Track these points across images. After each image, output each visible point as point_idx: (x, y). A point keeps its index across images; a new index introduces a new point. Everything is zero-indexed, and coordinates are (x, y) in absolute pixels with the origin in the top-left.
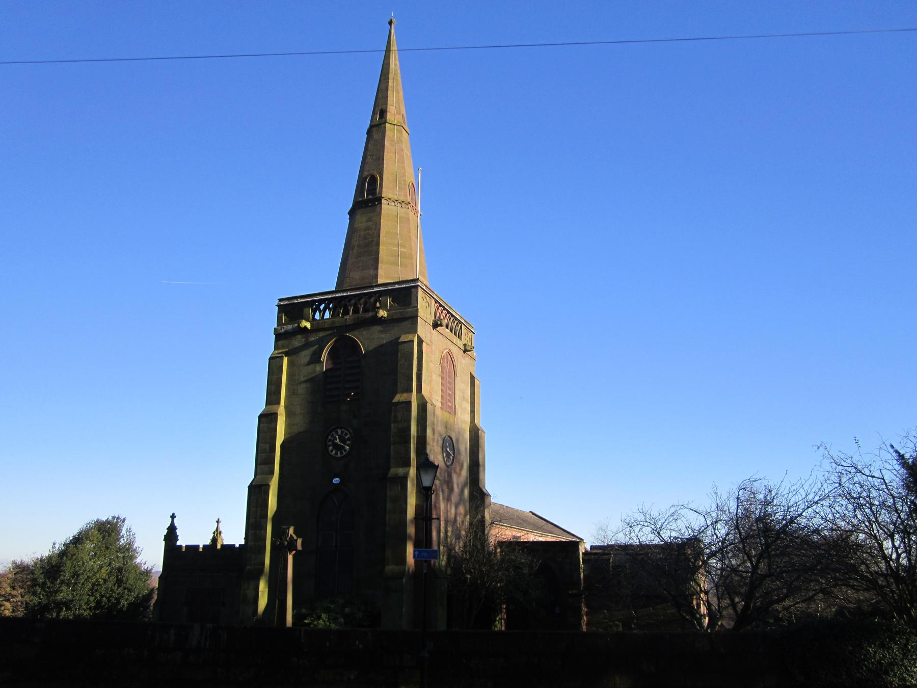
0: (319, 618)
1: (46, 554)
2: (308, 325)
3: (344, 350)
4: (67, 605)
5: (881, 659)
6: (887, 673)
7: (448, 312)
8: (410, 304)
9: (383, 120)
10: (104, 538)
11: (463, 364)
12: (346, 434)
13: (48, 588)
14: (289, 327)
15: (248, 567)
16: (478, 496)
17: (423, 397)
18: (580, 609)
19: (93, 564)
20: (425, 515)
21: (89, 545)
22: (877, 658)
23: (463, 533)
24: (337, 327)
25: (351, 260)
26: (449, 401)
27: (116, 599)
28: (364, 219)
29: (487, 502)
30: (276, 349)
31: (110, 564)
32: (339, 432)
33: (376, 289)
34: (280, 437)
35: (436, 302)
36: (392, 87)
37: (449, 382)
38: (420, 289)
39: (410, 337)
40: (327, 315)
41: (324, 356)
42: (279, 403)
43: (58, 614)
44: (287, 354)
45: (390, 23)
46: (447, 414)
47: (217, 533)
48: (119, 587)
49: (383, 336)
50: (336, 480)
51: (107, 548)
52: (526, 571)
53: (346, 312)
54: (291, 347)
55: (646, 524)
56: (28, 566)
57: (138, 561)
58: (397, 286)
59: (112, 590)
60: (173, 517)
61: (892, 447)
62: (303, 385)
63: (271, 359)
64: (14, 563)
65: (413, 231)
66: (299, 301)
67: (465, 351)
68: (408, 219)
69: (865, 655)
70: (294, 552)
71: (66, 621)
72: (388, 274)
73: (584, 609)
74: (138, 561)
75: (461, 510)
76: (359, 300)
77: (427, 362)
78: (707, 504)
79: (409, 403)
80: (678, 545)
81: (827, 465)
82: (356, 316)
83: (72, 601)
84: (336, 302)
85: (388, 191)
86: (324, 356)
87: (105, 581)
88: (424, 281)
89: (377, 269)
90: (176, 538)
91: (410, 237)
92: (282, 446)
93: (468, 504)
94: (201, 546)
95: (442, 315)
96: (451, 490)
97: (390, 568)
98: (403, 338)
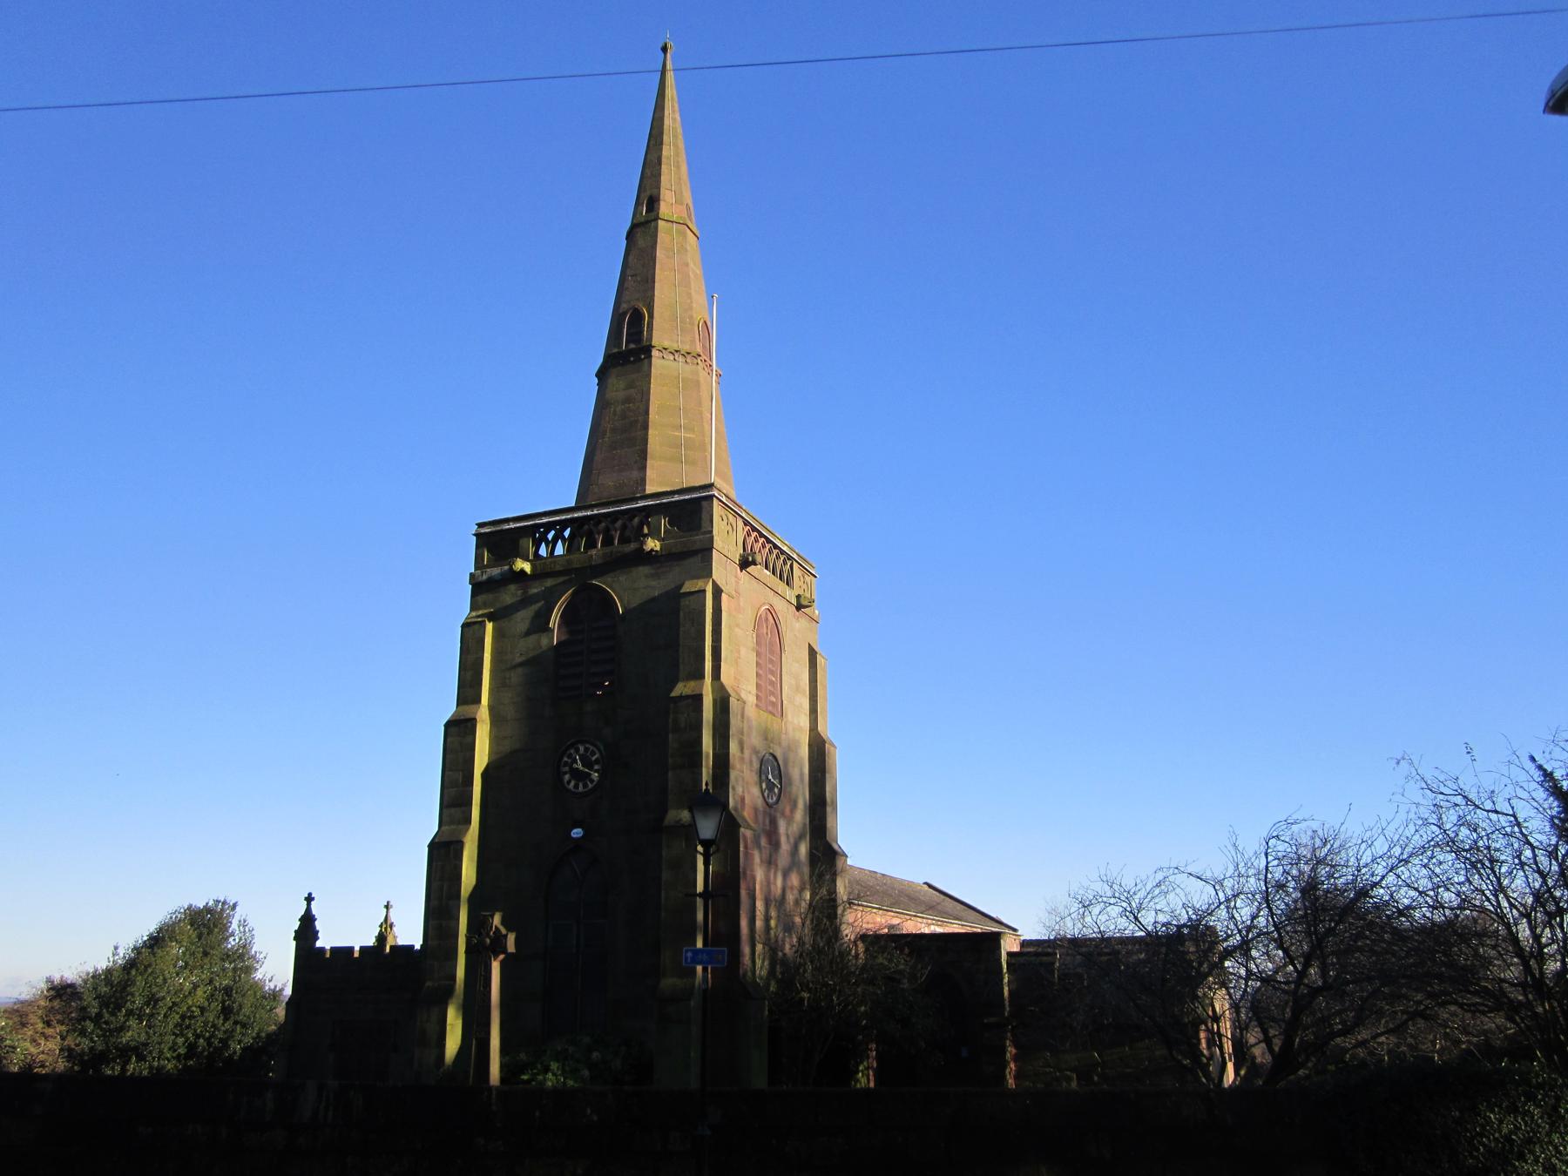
0: (547, 1070)
1: (103, 965)
2: (527, 567)
3: (589, 610)
4: (138, 1051)
5: (1511, 1132)
6: (1522, 1157)
7: (769, 541)
8: (699, 527)
9: (652, 215)
10: (200, 937)
11: (796, 629)
12: (593, 753)
13: (106, 1023)
14: (495, 571)
15: (428, 984)
16: (825, 857)
17: (722, 686)
18: (1004, 1052)
19: (182, 980)
20: (727, 888)
21: (176, 950)
22: (1505, 1131)
23: (798, 920)
25: (598, 457)
26: (772, 693)
27: (221, 1040)
28: (622, 385)
29: (839, 864)
30: (472, 609)
31: (211, 981)
32: (582, 749)
33: (641, 504)
34: (481, 759)
35: (746, 523)
36: (669, 158)
37: (771, 661)
39: (699, 584)
40: (560, 550)
41: (555, 620)
42: (478, 701)
43: (124, 1070)
44: (491, 617)
45: (664, 49)
46: (765, 715)
47: (387, 925)
48: (226, 1020)
49: (653, 583)
50: (577, 833)
51: (206, 954)
52: (905, 984)
53: (591, 544)
54: (498, 605)
55: (1113, 901)
56: (72, 986)
57: (258, 975)
58: (677, 498)
59: (214, 1026)
60: (309, 899)
61: (1533, 759)
62: (520, 670)
63: (464, 626)
64: (49, 980)
65: (706, 404)
66: (512, 526)
67: (799, 607)
68: (697, 384)
69: (1483, 1127)
70: (502, 957)
71: (137, 1080)
72: (662, 476)
73: (1011, 1050)
74: (258, 975)
75: (794, 880)
76: (631, 519)
77: (730, 627)
78: (1218, 864)
79: (698, 699)
80: (1168, 937)
81: (1415, 793)
82: (608, 550)
83: (146, 1045)
84: (574, 527)
85: (662, 334)
86: (555, 620)
87: (202, 1009)
88: (725, 487)
89: (644, 468)
90: (315, 935)
91: (701, 413)
92: (485, 775)
93: (806, 870)
94: (357, 949)
95: (757, 546)
96: (775, 845)
97: (668, 983)
98: (689, 587)
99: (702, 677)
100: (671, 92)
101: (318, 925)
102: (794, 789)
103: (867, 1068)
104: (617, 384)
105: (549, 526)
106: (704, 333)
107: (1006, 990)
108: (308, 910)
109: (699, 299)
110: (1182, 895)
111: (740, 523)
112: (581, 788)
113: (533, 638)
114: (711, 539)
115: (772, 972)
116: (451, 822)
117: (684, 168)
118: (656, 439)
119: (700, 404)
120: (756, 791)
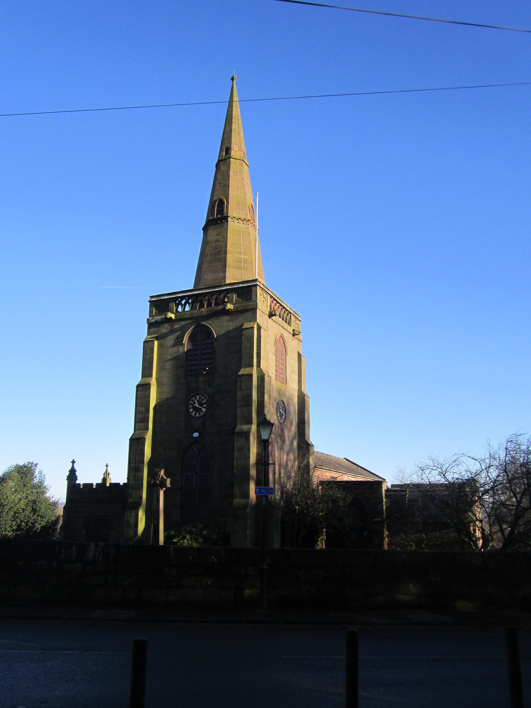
0: (184, 538)
2: (173, 316)
3: (201, 335)
7: (281, 305)
8: (251, 299)
9: (228, 156)
10: (22, 478)
12: (203, 400)
14: (158, 318)
15: (130, 500)
17: (261, 370)
18: (383, 533)
20: (264, 462)
21: (11, 484)
24: (195, 317)
25: (205, 266)
26: (282, 374)
27: (32, 523)
28: (215, 233)
30: (148, 334)
31: (27, 498)
32: (198, 397)
33: (224, 288)
35: (271, 297)
38: (258, 286)
40: (187, 308)
44: (157, 338)
45: (233, 79)
46: (279, 383)
47: (107, 474)
48: (34, 514)
49: (230, 324)
50: (196, 435)
51: (25, 486)
53: (202, 306)
54: (160, 333)
55: (434, 468)
57: (47, 495)
58: (241, 285)
59: (29, 517)
60: (73, 462)
62: (170, 362)
65: (253, 242)
66: (166, 297)
67: (294, 335)
70: (164, 489)
73: (386, 533)
74: (47, 495)
75: (291, 457)
76: (220, 295)
79: (251, 376)
80: (459, 484)
82: (209, 308)
84: (194, 298)
85: (233, 211)
87: (24, 510)
88: (262, 281)
90: (76, 478)
91: (250, 247)
93: (296, 453)
94: (95, 484)
95: (276, 307)
96: (283, 441)
97: (237, 501)
99: (252, 366)
100: (237, 126)
101: (77, 474)
102: (291, 416)
103: (322, 540)
104: (213, 233)
105: (183, 298)
106: (251, 210)
107: (384, 507)
108: (73, 467)
109: (249, 195)
110: (465, 466)
111: (269, 297)
112: (197, 415)
113: (176, 348)
114: (256, 304)
115: (282, 497)
116: (140, 429)
117: (242, 134)
118: (230, 259)
119: (250, 242)
120: (275, 417)
